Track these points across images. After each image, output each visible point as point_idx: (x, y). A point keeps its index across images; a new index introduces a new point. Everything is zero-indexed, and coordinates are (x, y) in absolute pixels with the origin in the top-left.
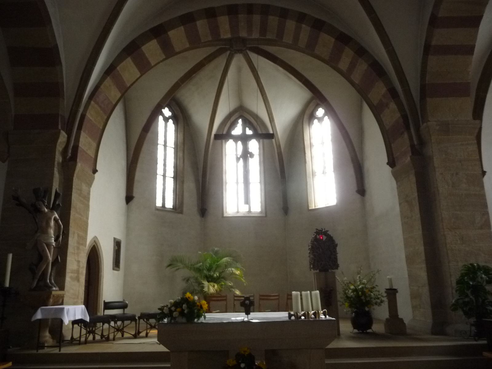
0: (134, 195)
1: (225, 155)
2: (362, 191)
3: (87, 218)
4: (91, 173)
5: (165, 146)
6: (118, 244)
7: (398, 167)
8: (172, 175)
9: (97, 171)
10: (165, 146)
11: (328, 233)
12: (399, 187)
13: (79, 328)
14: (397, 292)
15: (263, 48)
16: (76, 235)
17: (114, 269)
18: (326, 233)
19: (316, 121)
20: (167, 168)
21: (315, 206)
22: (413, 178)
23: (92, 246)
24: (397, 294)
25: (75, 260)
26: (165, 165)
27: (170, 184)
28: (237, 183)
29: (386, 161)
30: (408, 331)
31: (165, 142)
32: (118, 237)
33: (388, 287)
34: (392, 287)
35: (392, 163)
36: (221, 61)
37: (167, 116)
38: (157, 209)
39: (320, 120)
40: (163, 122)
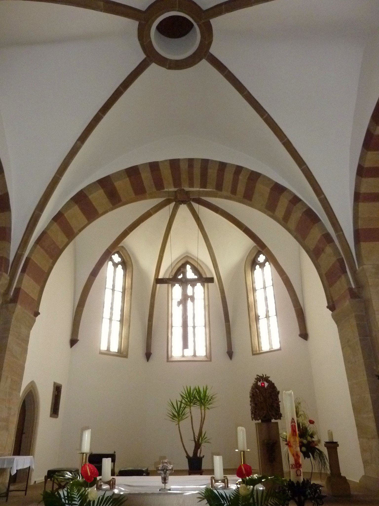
0: (79, 338)
1: (172, 299)
2: (304, 335)
3: (24, 362)
4: (32, 316)
5: (113, 290)
6: (58, 389)
7: (337, 310)
8: (119, 318)
9: (39, 314)
10: (113, 290)
11: (269, 379)
12: (340, 331)
13: (52, 482)
14: (338, 445)
15: (158, 199)
16: (9, 381)
17: (51, 416)
18: (266, 379)
19: (257, 267)
20: (114, 312)
21: (259, 351)
22: (353, 322)
23: (28, 391)
24: (338, 448)
25: (6, 407)
26: (112, 308)
27: (116, 326)
28: (194, 327)
29: (326, 304)
30: (353, 492)
31: (114, 286)
32: (59, 382)
33: (327, 440)
34: (333, 439)
35: (332, 307)
36: (167, 211)
37: (117, 262)
38: (102, 353)
39: (262, 265)
40: (113, 267)
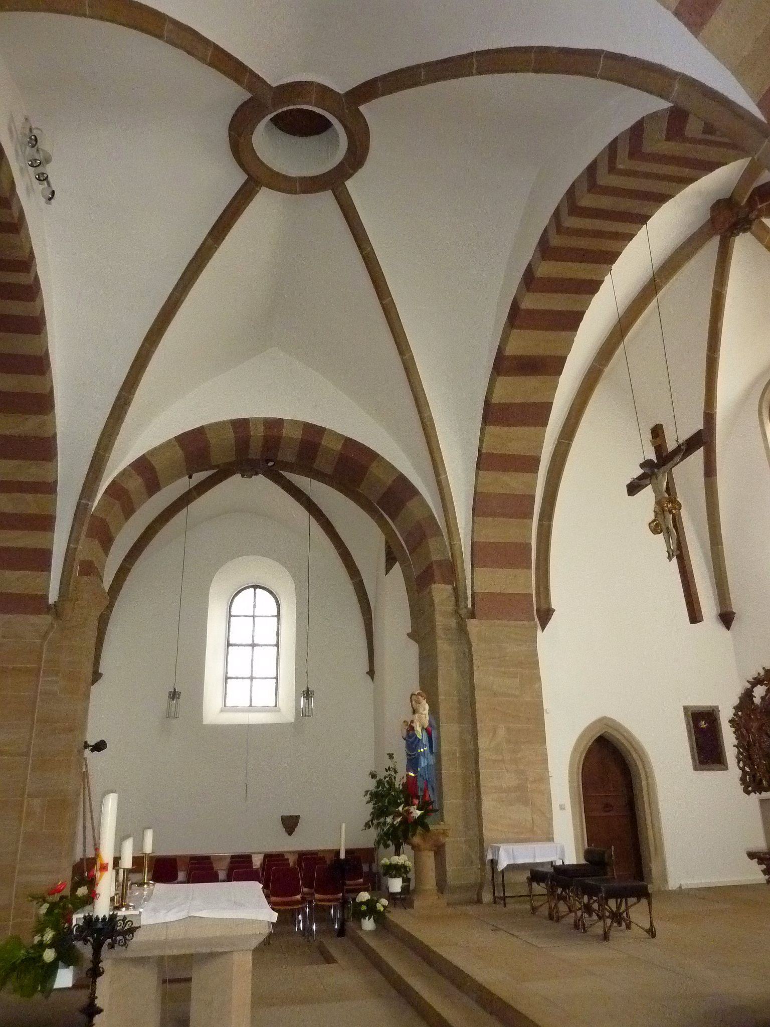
32: (703, 701)
